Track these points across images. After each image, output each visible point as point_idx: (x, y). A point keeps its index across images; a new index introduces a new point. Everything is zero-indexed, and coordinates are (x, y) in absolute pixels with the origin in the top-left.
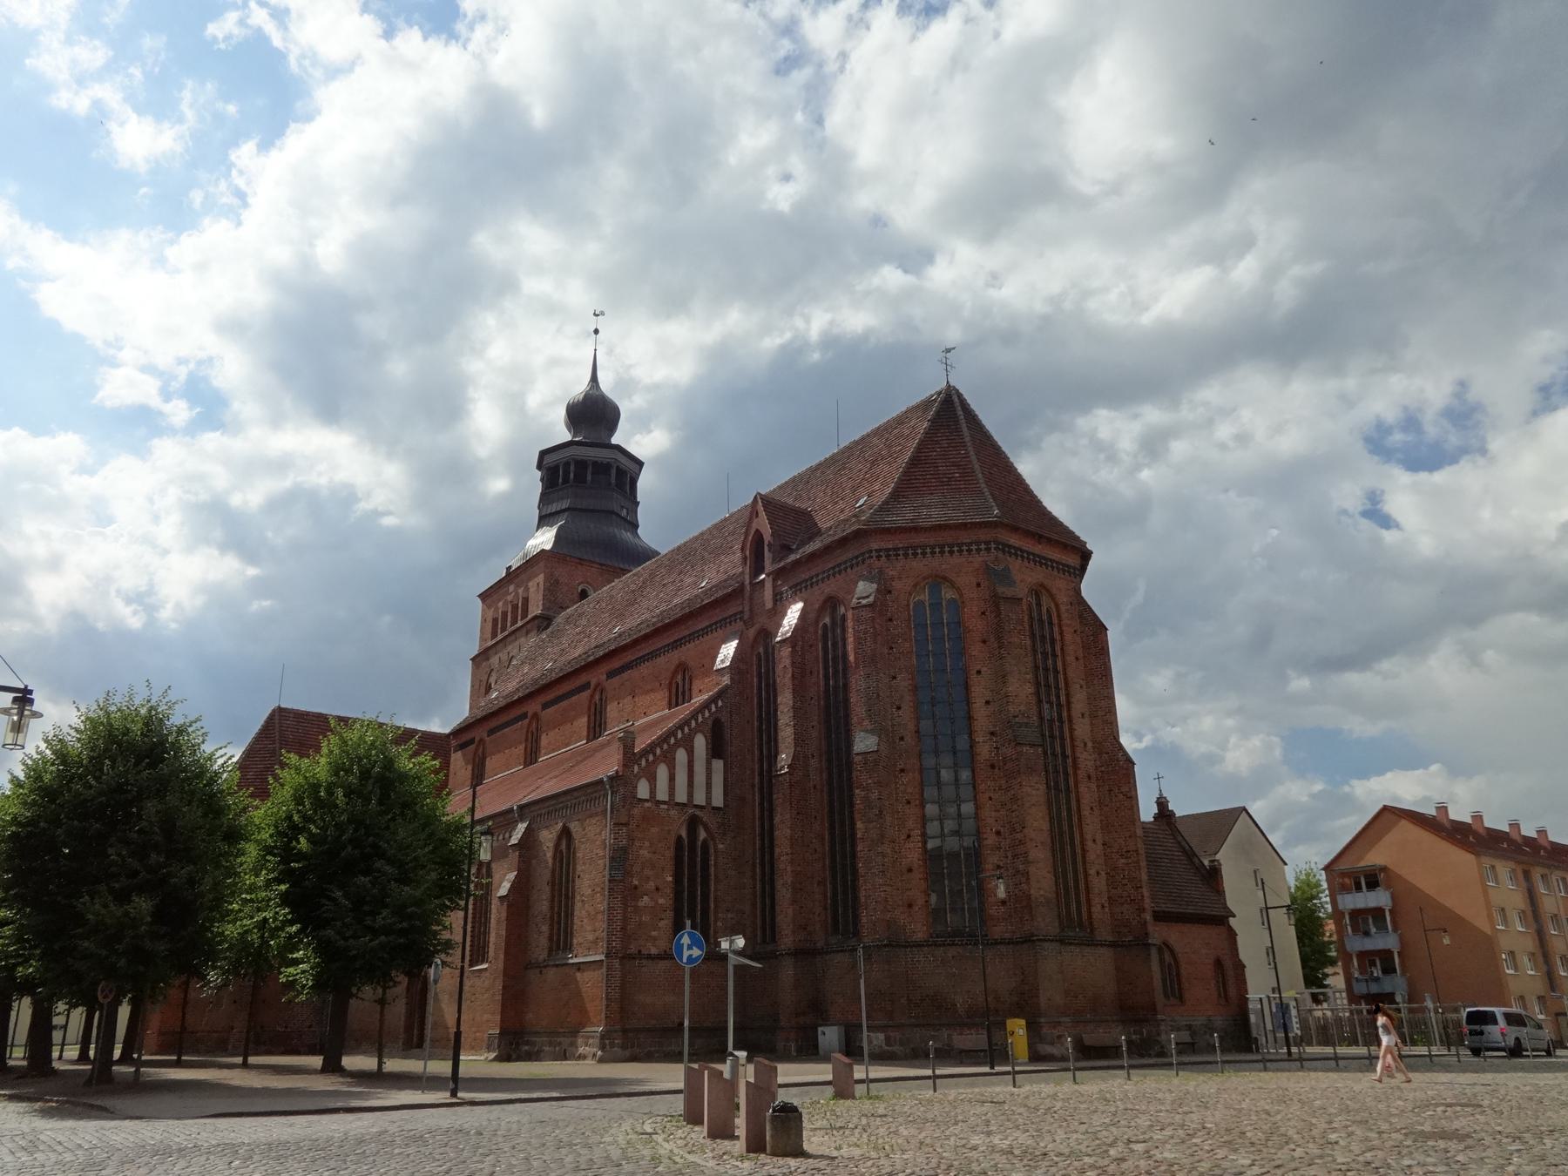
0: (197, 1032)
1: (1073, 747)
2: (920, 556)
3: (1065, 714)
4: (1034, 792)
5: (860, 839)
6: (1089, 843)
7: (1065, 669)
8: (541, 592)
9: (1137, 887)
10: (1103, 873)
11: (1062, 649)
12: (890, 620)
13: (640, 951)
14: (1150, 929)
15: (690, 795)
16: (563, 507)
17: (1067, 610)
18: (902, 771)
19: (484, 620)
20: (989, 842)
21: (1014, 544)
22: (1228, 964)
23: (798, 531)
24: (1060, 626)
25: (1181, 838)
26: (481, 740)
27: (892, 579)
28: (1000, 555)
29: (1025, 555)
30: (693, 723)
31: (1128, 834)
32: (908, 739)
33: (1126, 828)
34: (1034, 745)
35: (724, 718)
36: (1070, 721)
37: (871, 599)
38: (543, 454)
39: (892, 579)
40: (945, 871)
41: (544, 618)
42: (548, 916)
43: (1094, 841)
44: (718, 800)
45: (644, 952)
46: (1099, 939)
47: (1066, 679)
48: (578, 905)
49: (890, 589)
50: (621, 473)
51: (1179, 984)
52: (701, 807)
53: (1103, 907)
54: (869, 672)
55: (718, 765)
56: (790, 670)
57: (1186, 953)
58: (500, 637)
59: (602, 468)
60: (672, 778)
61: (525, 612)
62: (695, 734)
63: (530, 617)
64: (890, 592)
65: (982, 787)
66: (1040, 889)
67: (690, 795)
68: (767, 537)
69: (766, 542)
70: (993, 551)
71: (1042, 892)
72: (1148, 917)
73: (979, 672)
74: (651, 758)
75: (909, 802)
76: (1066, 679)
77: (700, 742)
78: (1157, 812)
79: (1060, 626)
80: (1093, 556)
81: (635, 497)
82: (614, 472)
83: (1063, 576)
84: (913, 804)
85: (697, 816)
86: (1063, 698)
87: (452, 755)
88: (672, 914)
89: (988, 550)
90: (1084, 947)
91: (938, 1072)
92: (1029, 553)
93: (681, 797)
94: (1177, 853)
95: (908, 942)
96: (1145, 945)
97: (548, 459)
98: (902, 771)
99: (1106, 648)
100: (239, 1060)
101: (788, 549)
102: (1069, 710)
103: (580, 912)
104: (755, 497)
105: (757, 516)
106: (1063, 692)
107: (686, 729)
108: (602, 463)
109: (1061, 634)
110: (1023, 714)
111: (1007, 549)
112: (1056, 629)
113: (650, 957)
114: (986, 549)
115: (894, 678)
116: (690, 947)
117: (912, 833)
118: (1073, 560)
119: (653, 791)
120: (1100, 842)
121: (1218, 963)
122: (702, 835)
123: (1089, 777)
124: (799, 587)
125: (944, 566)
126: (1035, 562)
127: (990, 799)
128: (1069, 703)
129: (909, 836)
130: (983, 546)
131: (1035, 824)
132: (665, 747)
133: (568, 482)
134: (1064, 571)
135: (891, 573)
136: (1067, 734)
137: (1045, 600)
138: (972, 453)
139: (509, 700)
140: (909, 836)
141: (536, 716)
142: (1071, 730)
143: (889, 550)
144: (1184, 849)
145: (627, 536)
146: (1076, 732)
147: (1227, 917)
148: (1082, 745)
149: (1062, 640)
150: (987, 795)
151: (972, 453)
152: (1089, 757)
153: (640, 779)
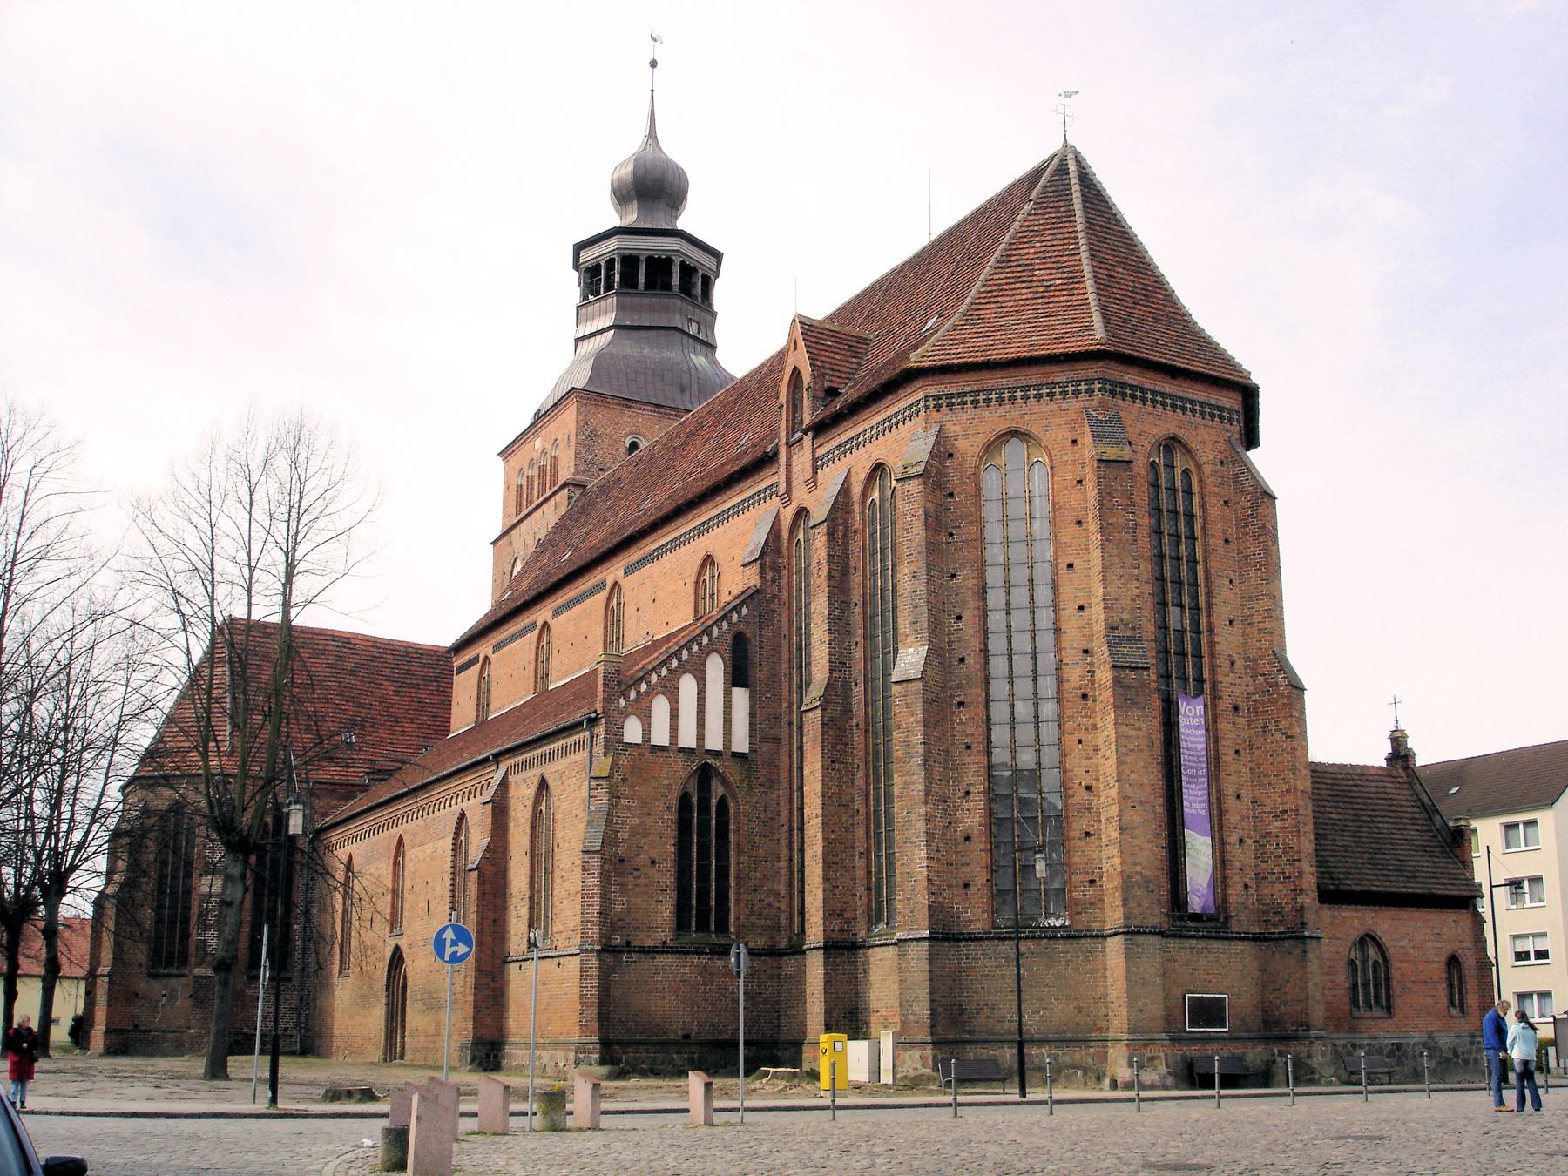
0: (150, 1031)
1: (1213, 667)
2: (994, 403)
3: (1203, 622)
4: (1133, 733)
5: (898, 797)
6: (1230, 802)
7: (1206, 557)
8: (573, 449)
9: (1294, 860)
10: (1250, 842)
11: (1204, 529)
12: (951, 495)
13: (628, 943)
14: (1309, 916)
15: (701, 737)
16: (607, 325)
17: (1214, 473)
18: (961, 704)
19: (507, 488)
20: (1077, 800)
21: (1130, 382)
22: (1468, 960)
23: (855, 366)
24: (1203, 496)
25: (1420, 788)
26: (486, 658)
27: (956, 437)
28: (1107, 397)
29: (1149, 396)
30: (705, 640)
31: (1286, 787)
32: (969, 660)
33: (1284, 779)
34: (1137, 668)
35: (749, 632)
36: (1211, 630)
37: (921, 469)
38: (579, 248)
39: (956, 437)
40: (1016, 839)
41: (575, 485)
42: (527, 896)
43: (1238, 797)
44: (741, 744)
45: (635, 943)
46: (1236, 930)
47: (1207, 572)
48: (558, 881)
49: (950, 451)
50: (688, 271)
51: (1388, 988)
52: (717, 754)
53: (1246, 886)
54: (916, 570)
55: (740, 696)
56: (826, 565)
57: (1403, 947)
58: (525, 512)
59: (659, 267)
60: (674, 715)
61: (555, 475)
62: (708, 655)
63: (560, 483)
64: (951, 455)
65: (1069, 726)
66: (1135, 864)
67: (701, 737)
68: (807, 378)
69: (805, 386)
70: (1096, 392)
71: (1139, 868)
72: (1309, 899)
73: (1070, 566)
74: (644, 687)
75: (968, 747)
76: (1207, 572)
77: (716, 669)
78: (1390, 751)
79: (1203, 496)
80: (1261, 391)
81: (710, 305)
82: (676, 270)
83: (1211, 423)
84: (974, 749)
85: (710, 765)
86: (1202, 600)
87: (455, 677)
88: (674, 895)
89: (1090, 391)
90: (1211, 942)
91: (961, 1099)
92: (1154, 393)
93: (688, 739)
94: (1409, 810)
95: (963, 934)
96: (1297, 938)
97: (587, 256)
98: (961, 704)
99: (1269, 526)
100: (1001, 1091)
101: (832, 393)
102: (1209, 615)
103: (560, 891)
104: (794, 320)
105: (795, 349)
106: (1202, 590)
107: (695, 648)
108: (660, 258)
109: (1204, 507)
110: (1126, 625)
111: (1118, 389)
112: (1196, 499)
113: (644, 950)
114: (1087, 391)
115: (954, 576)
116: (454, 943)
117: (972, 789)
118: (1231, 401)
119: (647, 733)
120: (1246, 799)
121: (1453, 961)
122: (718, 790)
123: (1236, 708)
124: (843, 449)
125: (1027, 417)
126: (1164, 404)
127: (1080, 741)
128: (1209, 605)
129: (967, 793)
130: (1083, 387)
131: (1133, 776)
132: (664, 672)
133: (613, 288)
134: (1212, 416)
135: (953, 428)
136: (1205, 650)
137: (1180, 462)
138: (1083, 248)
139: (514, 605)
140: (967, 793)
141: (546, 625)
142: (1212, 644)
143: (952, 396)
144: (1423, 804)
145: (700, 360)
146: (1217, 647)
147: (1475, 897)
148: (1227, 664)
149: (1204, 516)
150: (1076, 737)
151: (1083, 248)
152: (1238, 681)
153: (627, 716)
